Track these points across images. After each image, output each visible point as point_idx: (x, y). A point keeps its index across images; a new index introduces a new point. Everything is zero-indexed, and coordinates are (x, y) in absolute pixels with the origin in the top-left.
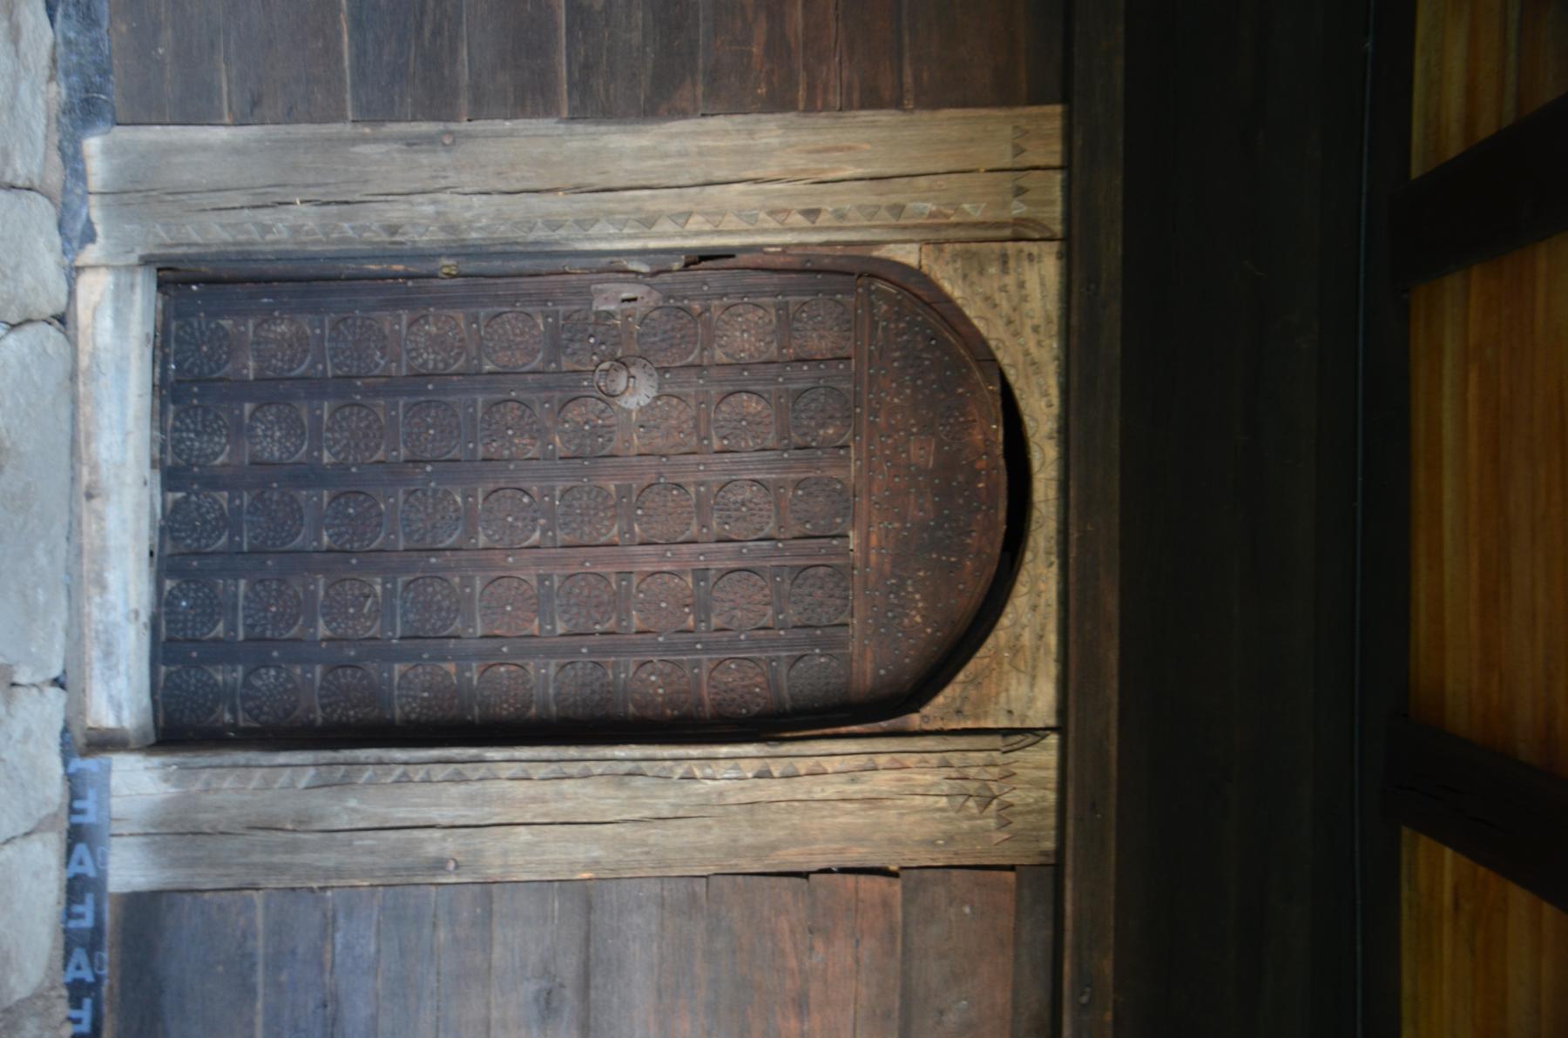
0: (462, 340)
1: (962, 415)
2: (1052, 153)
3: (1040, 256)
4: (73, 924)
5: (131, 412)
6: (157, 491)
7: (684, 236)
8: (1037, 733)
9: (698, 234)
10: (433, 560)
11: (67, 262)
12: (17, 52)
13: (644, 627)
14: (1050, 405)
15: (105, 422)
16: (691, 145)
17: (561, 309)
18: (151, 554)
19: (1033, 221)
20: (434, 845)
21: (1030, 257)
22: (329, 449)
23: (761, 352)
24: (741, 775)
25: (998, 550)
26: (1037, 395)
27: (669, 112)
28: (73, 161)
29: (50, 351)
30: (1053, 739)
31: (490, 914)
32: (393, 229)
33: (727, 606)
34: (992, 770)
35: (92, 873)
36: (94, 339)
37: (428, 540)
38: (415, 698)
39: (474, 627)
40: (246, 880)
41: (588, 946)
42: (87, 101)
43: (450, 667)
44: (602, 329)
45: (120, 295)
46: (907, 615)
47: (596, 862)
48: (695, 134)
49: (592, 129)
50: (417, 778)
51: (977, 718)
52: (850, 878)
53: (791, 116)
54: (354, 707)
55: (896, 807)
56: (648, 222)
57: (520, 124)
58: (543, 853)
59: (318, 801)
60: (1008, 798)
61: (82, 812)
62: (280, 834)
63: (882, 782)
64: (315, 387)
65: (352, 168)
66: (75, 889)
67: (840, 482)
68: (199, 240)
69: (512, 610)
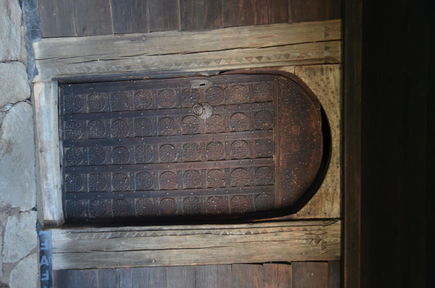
0: (151, 99)
1: (308, 118)
2: (337, 35)
3: (334, 69)
4: (43, 279)
5: (52, 126)
6: (62, 147)
7: (219, 67)
8: (333, 220)
9: (223, 66)
10: (145, 167)
11: (30, 82)
12: (10, 18)
13: (210, 186)
14: (337, 117)
15: (44, 129)
16: (221, 37)
17: (182, 88)
18: (61, 166)
19: (331, 58)
20: (148, 255)
21: (331, 69)
22: (112, 133)
23: (244, 100)
24: (241, 233)
25: (320, 161)
26: (333, 114)
27: (213, 27)
28: (30, 50)
29: (26, 110)
30: (339, 222)
31: (166, 276)
32: (128, 67)
33: (235, 179)
34: (320, 231)
35: (48, 264)
36: (40, 104)
37: (143, 161)
38: (141, 209)
39: (158, 187)
40: (93, 266)
41: (196, 285)
42: (33, 31)
43: (151, 199)
44: (194, 94)
45: (47, 90)
46: (292, 182)
47: (197, 260)
48: (222, 33)
49: (189, 33)
50: (142, 235)
51: (315, 215)
52: (276, 265)
53: (252, 27)
54: (123, 212)
55: (290, 243)
56: (207, 62)
57: (166, 33)
58: (181, 257)
59: (113, 242)
60: (325, 240)
61: (44, 246)
62: (102, 252)
63: (285, 235)
64: (107, 115)
65: (115, 49)
66: (43, 269)
67: (270, 140)
68: (69, 73)
69: (170, 184)
